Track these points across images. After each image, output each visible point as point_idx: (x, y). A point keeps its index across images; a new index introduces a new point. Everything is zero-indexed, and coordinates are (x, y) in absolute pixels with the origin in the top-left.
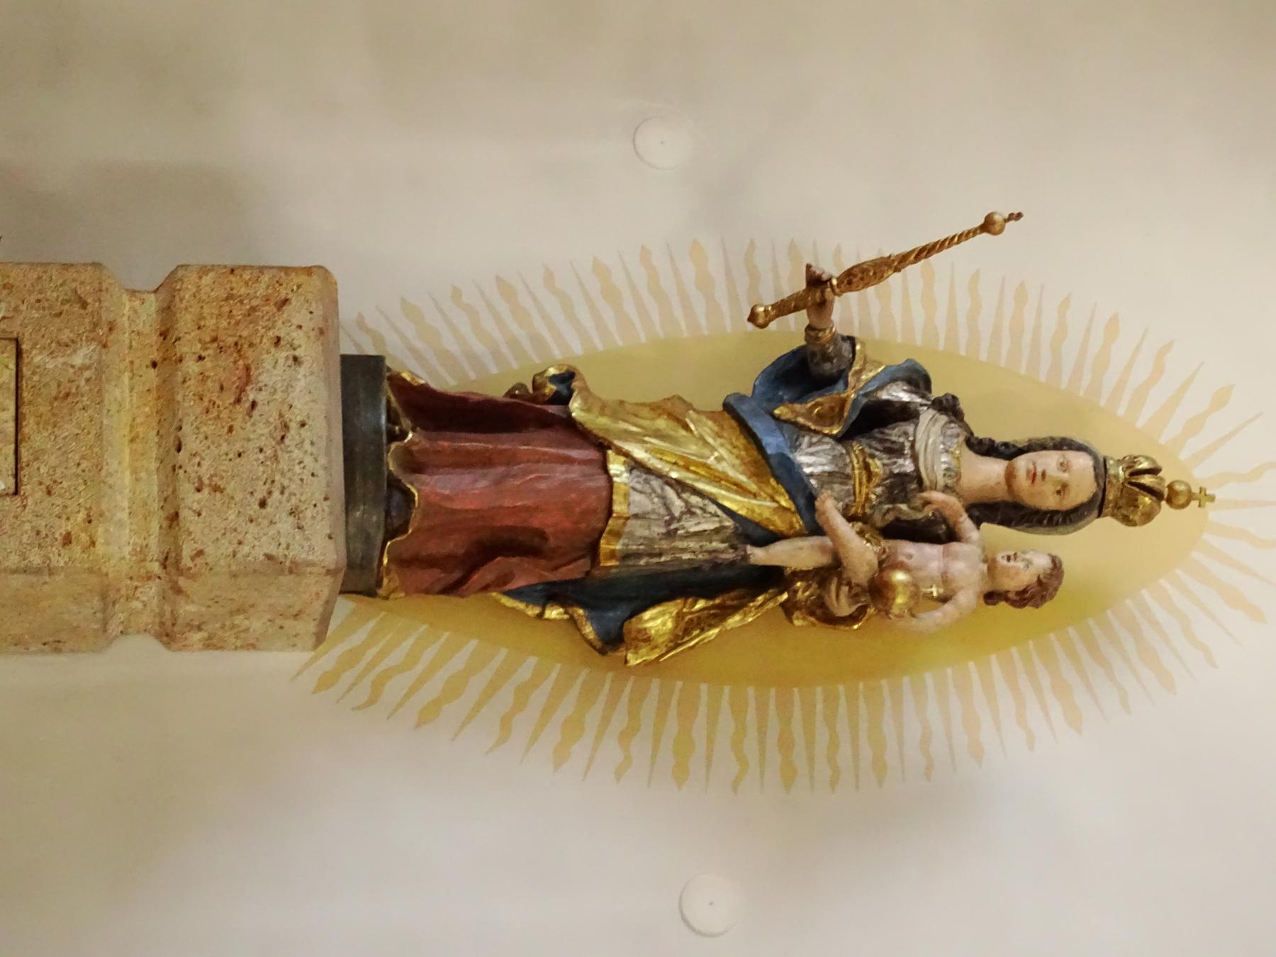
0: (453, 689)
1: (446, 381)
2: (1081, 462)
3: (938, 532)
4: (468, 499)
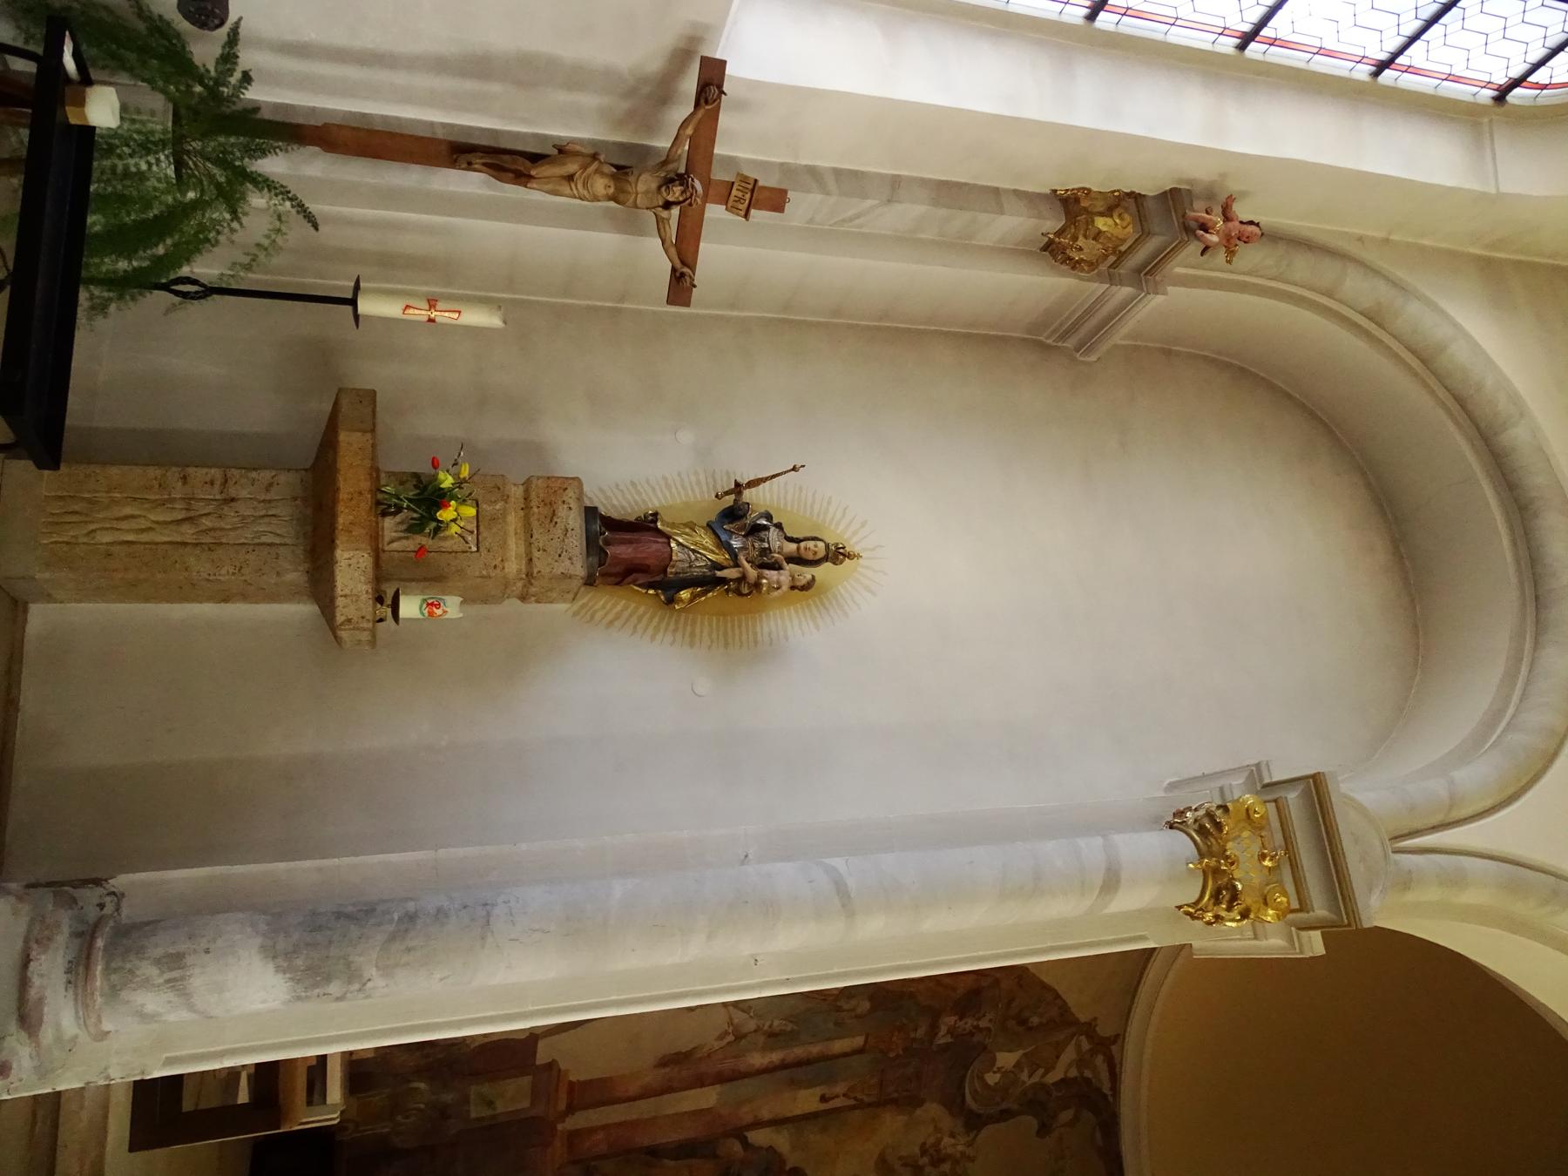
0: (617, 617)
1: (615, 515)
2: (821, 545)
3: (776, 567)
4: (628, 557)
